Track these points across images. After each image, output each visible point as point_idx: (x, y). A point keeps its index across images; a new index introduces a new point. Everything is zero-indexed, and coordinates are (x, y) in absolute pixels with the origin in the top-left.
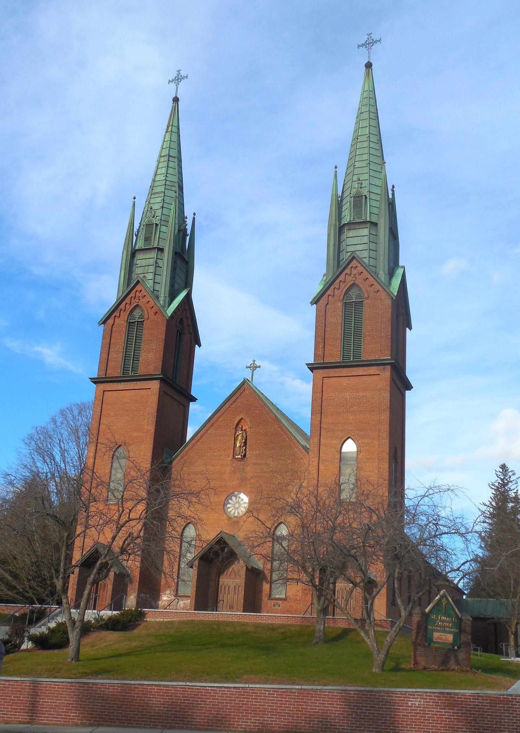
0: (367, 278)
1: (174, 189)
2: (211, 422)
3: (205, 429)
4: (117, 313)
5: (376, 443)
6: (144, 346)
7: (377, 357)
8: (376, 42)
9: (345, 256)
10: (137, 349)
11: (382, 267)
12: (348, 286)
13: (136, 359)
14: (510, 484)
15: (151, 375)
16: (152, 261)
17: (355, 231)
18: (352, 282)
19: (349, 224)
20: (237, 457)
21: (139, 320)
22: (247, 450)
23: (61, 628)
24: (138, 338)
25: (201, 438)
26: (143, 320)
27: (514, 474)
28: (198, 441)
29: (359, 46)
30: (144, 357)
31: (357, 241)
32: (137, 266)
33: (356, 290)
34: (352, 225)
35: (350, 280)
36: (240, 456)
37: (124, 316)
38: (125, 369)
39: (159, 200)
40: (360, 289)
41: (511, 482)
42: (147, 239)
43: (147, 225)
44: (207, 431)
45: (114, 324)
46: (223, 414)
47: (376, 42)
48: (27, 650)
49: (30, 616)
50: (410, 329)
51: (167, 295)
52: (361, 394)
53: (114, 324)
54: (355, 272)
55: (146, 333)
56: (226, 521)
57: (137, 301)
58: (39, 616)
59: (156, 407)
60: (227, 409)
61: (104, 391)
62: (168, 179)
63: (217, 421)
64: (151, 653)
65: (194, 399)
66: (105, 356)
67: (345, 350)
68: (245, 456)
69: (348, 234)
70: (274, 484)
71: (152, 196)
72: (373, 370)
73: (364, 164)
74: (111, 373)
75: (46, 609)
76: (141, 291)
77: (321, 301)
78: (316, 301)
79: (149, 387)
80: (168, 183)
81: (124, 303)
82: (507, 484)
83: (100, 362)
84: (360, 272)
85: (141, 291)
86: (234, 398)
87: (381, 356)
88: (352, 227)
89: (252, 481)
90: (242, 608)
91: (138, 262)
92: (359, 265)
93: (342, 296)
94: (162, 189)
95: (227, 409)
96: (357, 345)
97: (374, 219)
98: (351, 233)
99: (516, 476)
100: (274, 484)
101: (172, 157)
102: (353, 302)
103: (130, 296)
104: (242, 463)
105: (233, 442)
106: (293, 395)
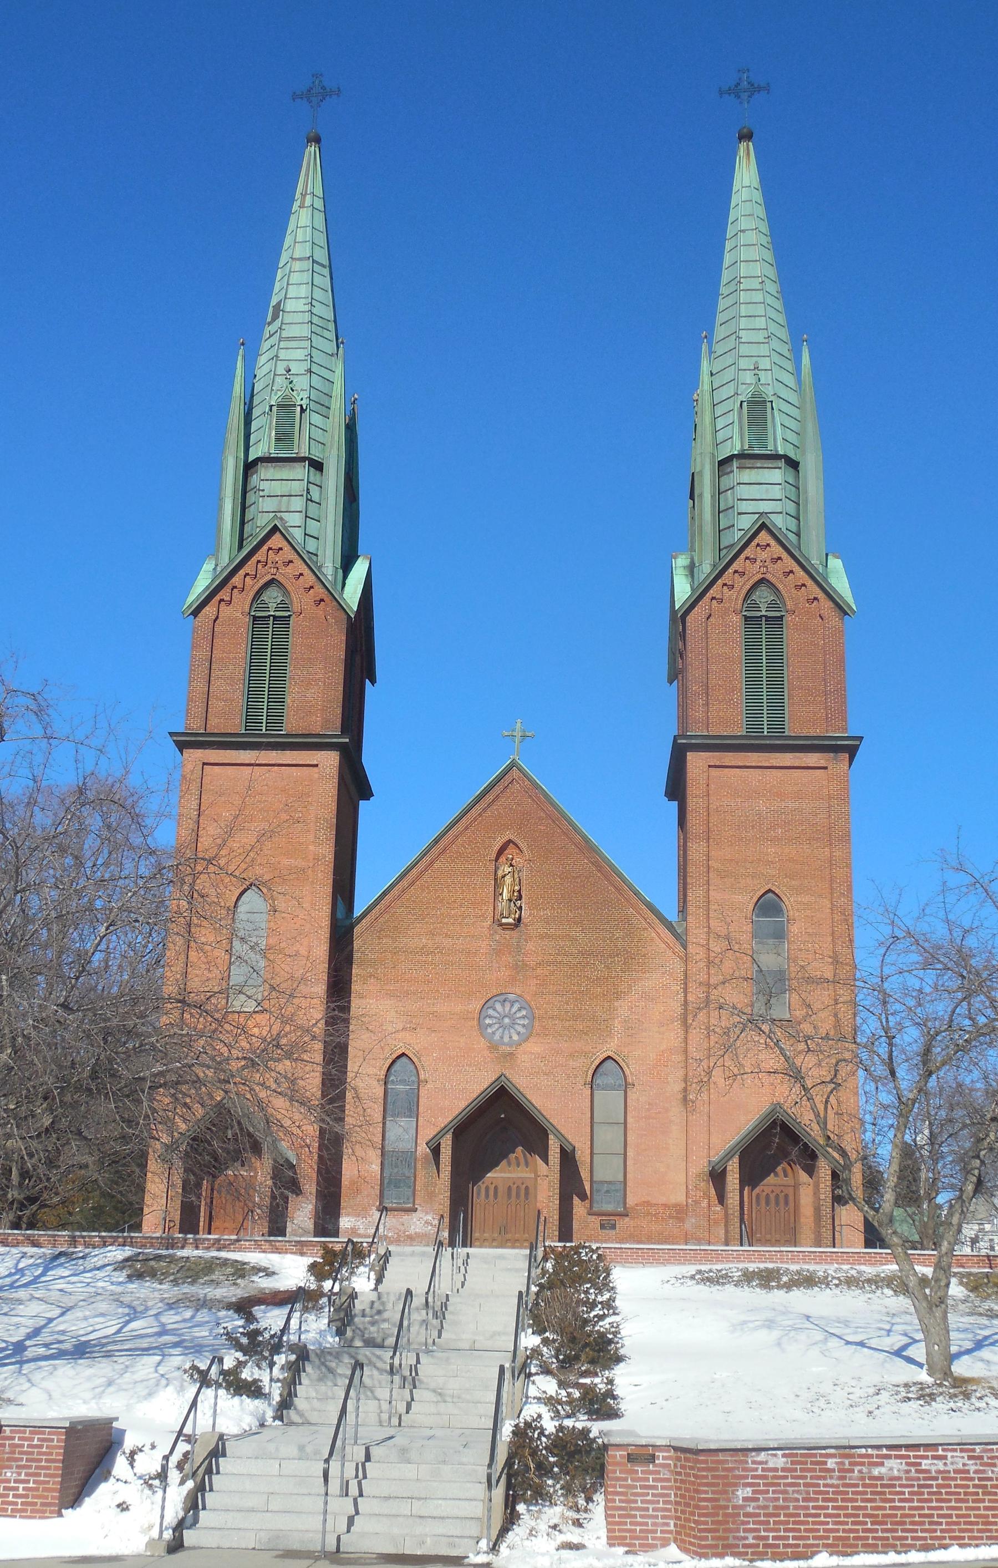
0: (301, 574)
1: (326, 334)
2: (442, 844)
3: (428, 858)
4: (224, 594)
5: (827, 903)
7: (818, 732)
9: (260, 522)
10: (278, 676)
11: (329, 552)
12: (751, 582)
13: (277, 697)
16: (297, 487)
17: (754, 471)
18: (269, 577)
19: (742, 456)
20: (504, 921)
21: (278, 614)
24: (281, 652)
25: (418, 877)
26: (778, 614)
28: (413, 883)
30: (293, 695)
32: (261, 493)
33: (766, 594)
35: (755, 572)
36: (510, 920)
37: (242, 602)
38: (251, 718)
39: (300, 354)
40: (286, 592)
42: (283, 437)
44: (432, 862)
45: (217, 618)
46: (467, 828)
50: (373, 682)
51: (338, 565)
52: (791, 805)
53: (217, 618)
54: (764, 555)
55: (296, 642)
56: (486, 1053)
57: (273, 571)
59: (334, 806)
60: (475, 819)
61: (204, 764)
62: (314, 311)
67: (753, 714)
68: (519, 920)
69: (265, 472)
70: (589, 979)
71: (282, 344)
72: (813, 759)
73: (760, 336)
74: (217, 724)
76: (281, 549)
78: (196, 613)
79: (315, 762)
80: (315, 320)
81: (242, 572)
84: (775, 556)
85: (281, 549)
86: (490, 797)
87: (827, 731)
88: (748, 463)
89: (539, 971)
90: (557, 1233)
92: (773, 543)
93: (740, 602)
94: (305, 331)
95: (475, 819)
96: (777, 707)
97: (316, 454)
98: (747, 476)
100: (589, 979)
101: (318, 263)
102: (761, 617)
103: (254, 559)
104: (514, 934)
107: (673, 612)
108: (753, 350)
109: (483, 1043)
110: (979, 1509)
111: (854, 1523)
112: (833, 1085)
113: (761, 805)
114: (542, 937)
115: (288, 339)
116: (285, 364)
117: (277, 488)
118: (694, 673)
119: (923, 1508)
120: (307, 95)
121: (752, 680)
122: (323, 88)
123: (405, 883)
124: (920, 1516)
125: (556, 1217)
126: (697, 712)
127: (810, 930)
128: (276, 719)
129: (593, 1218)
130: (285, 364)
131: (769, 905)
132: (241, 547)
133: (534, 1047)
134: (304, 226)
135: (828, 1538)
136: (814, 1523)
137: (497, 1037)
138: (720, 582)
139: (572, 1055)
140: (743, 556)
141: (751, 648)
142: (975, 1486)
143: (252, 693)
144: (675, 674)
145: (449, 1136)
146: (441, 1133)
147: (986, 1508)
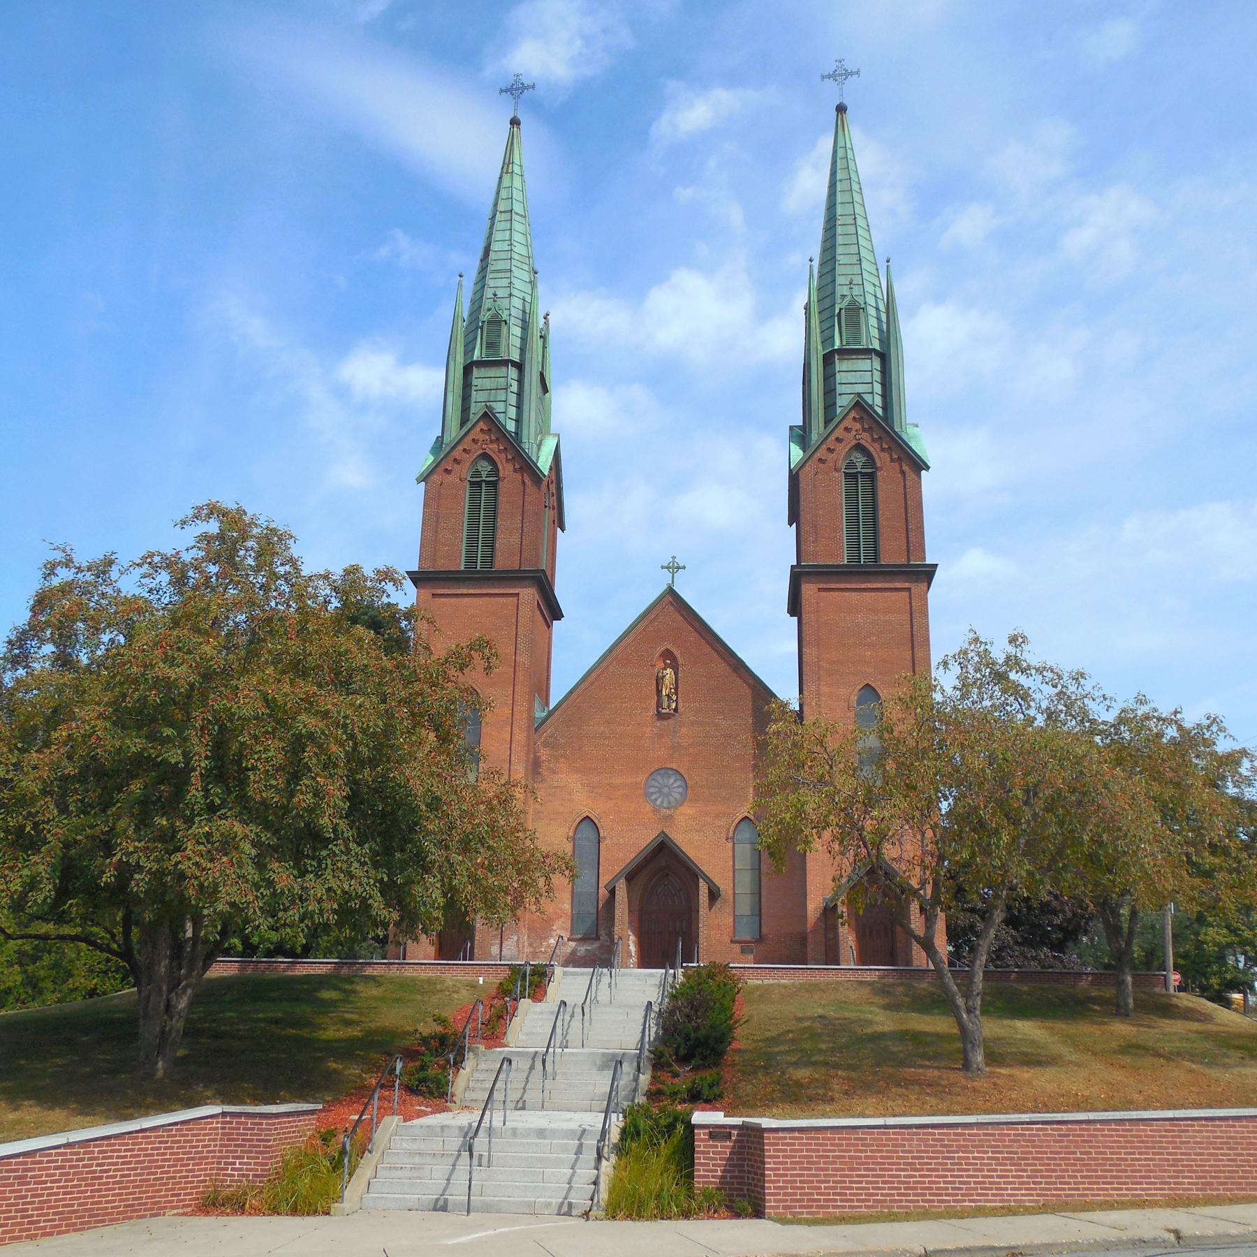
8: (851, 74)
13: (491, 545)
15: (519, 571)
18: (481, 451)
22: (680, 701)
34: (845, 353)
38: (471, 560)
47: (851, 74)
67: (855, 546)
74: (443, 565)
78: (425, 478)
91: (475, 382)
105: (654, 687)
107: (790, 471)
108: (848, 270)
109: (648, 808)
110: (992, 1177)
111: (890, 1188)
116: (493, 290)
117: (487, 384)
118: (805, 516)
119: (946, 1176)
120: (848, 74)
121: (853, 522)
124: (945, 1182)
126: (809, 547)
128: (490, 558)
129: (733, 945)
130: (493, 290)
131: (869, 691)
132: (463, 424)
133: (688, 810)
135: (868, 1201)
136: (857, 1188)
137: (658, 802)
138: (824, 446)
139: (717, 816)
140: (842, 426)
141: (852, 497)
142: (989, 1158)
143: (472, 541)
144: (794, 517)
145: (623, 880)
146: (616, 879)
147: (998, 1177)
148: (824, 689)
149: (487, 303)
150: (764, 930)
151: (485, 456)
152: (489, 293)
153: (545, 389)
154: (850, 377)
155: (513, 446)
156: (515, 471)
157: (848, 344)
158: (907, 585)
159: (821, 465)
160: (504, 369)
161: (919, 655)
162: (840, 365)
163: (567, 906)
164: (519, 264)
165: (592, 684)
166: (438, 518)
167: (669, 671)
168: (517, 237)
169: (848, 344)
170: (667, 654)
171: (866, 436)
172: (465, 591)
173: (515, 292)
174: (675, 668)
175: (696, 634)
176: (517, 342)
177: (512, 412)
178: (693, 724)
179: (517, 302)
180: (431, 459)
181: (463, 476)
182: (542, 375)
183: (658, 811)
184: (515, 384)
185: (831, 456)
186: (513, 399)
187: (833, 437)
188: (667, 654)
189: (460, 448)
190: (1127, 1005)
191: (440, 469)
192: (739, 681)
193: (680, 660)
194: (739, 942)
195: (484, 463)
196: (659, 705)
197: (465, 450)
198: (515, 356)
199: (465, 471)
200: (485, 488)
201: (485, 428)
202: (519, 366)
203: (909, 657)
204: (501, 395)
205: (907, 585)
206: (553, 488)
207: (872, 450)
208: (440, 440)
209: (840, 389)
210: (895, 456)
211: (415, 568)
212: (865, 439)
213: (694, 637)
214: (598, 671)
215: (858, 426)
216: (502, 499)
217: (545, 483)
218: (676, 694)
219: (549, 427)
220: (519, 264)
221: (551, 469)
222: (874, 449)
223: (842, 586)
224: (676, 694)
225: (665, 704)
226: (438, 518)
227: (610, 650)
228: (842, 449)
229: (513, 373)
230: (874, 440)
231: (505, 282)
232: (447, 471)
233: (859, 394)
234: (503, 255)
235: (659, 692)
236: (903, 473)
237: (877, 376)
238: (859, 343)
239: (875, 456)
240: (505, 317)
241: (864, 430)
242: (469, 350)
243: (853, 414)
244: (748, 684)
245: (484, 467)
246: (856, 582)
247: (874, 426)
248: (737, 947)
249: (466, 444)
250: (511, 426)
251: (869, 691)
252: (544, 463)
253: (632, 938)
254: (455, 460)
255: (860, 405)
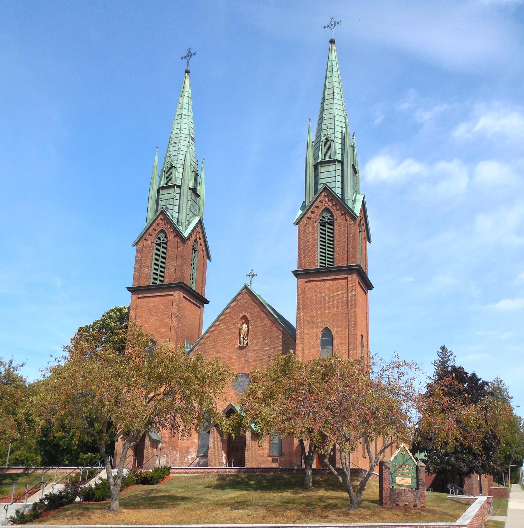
3: (216, 324)
6: (168, 261)
8: (337, 23)
10: (164, 264)
13: (163, 272)
14: (449, 362)
15: (174, 284)
18: (160, 229)
23: (105, 484)
24: (165, 255)
27: (452, 354)
28: (211, 334)
29: (325, 27)
31: (330, 176)
34: (324, 163)
38: (155, 280)
41: (450, 360)
43: (168, 168)
44: (218, 325)
47: (337, 23)
48: (78, 503)
49: (82, 476)
56: (234, 396)
58: (92, 475)
63: (225, 317)
64: (99, 497)
65: (207, 302)
66: (138, 270)
67: (323, 259)
74: (143, 283)
75: (95, 469)
77: (302, 222)
78: (298, 223)
80: (183, 135)
82: (447, 362)
83: (134, 275)
99: (454, 355)
105: (238, 333)
106: (284, 298)
112: (258, 404)
113: (324, 295)
114: (254, 351)
115: (173, 143)
120: (329, 26)
121: (323, 247)
122: (335, 22)
123: (208, 334)
125: (336, 460)
127: (341, 342)
128: (162, 278)
129: (269, 458)
131: (327, 332)
134: (186, 103)
138: (310, 211)
140: (318, 200)
141: (323, 234)
143: (156, 270)
148: (306, 331)
149: (324, 132)
150: (283, 451)
151: (162, 231)
152: (324, 127)
153: (355, 172)
154: (326, 175)
155: (340, 203)
156: (174, 236)
157: (325, 158)
158: (346, 276)
159: (308, 220)
160: (173, 189)
161: (351, 311)
162: (320, 169)
163: (196, 440)
164: (184, 139)
165: (211, 334)
166: (141, 261)
167: (245, 325)
168: (184, 126)
169: (325, 158)
170: (244, 318)
171: (330, 204)
172: (151, 295)
173: (181, 152)
174: (247, 322)
175: (257, 307)
176: (340, 151)
177: (339, 185)
178: (254, 351)
179: (182, 157)
180: (300, 212)
181: (317, 220)
182: (353, 165)
183: (237, 394)
184: (178, 196)
185: (313, 215)
186: (177, 203)
187: (314, 206)
188: (244, 318)
189: (152, 228)
190: (308, 483)
191: (143, 239)
192: (276, 329)
193: (250, 320)
194: (271, 456)
195: (326, 213)
196: (240, 342)
197: (154, 229)
198: (339, 158)
199: (153, 239)
200: (327, 224)
201: (162, 218)
202: (342, 162)
203: (346, 312)
204: (171, 201)
205: (346, 276)
206: (363, 221)
207: (332, 210)
208: (304, 202)
209: (319, 182)
210: (343, 212)
211: (131, 286)
212: (330, 205)
213: (256, 309)
214: (213, 328)
215: (327, 199)
216: (169, 250)
217: (358, 219)
218: (248, 337)
219: (359, 191)
220: (184, 139)
221: (361, 212)
222: (333, 209)
223: (316, 279)
224: (248, 337)
225: (242, 342)
226: (141, 261)
227: (219, 317)
228: (318, 211)
229: (339, 166)
230: (333, 205)
231: (176, 148)
232: (146, 240)
233: (325, 184)
234: (177, 136)
235: (240, 336)
236: (346, 220)
237: (339, 173)
238: (330, 158)
239: (334, 213)
240: (174, 165)
241: (329, 201)
242: (316, 157)
243: (324, 193)
244: (280, 330)
245: (327, 215)
246: (323, 276)
247: (333, 198)
248: (270, 459)
249: (317, 203)
250: (338, 191)
251: (327, 332)
252: (357, 210)
253: (224, 455)
254: (149, 234)
255: (326, 189)
